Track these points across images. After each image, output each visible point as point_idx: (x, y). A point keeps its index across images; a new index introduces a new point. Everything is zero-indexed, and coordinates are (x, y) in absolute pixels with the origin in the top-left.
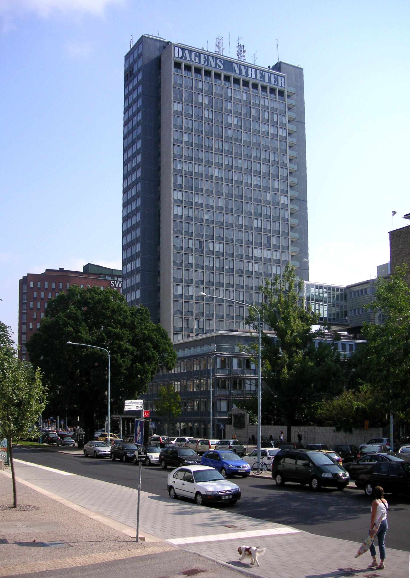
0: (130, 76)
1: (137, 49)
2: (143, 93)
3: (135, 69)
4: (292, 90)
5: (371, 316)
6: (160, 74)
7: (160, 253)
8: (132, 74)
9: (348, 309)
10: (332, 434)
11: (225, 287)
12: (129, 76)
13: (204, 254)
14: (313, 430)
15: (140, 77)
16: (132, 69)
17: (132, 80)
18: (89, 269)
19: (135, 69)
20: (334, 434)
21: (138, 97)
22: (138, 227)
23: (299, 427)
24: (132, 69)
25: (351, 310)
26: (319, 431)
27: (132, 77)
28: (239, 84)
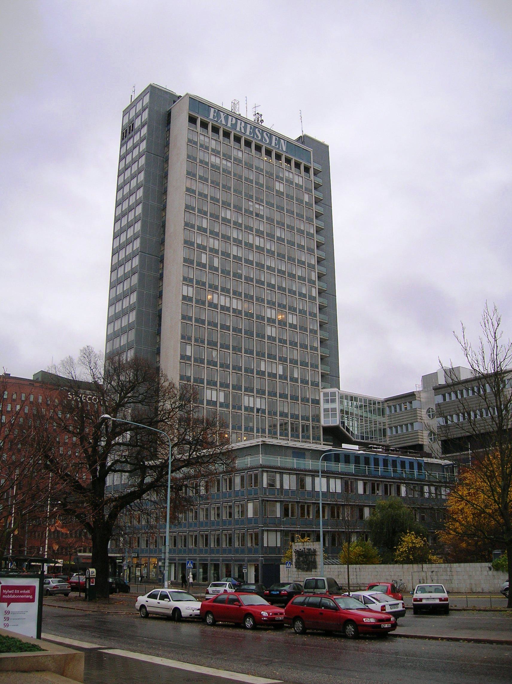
0: (130, 133)
1: (141, 101)
2: (148, 151)
3: (138, 123)
4: (319, 167)
5: (419, 434)
6: (169, 130)
7: (160, 345)
8: (132, 130)
9: (387, 427)
10: (485, 573)
11: (243, 390)
12: (127, 132)
13: (219, 347)
14: (448, 569)
15: (144, 131)
16: (133, 124)
17: (133, 137)
18: (303, 139)
19: (138, 123)
20: (490, 573)
21: (140, 156)
22: (132, 310)
23: (420, 566)
24: (133, 124)
25: (391, 428)
26: (459, 569)
27: (133, 133)
28: (260, 151)
